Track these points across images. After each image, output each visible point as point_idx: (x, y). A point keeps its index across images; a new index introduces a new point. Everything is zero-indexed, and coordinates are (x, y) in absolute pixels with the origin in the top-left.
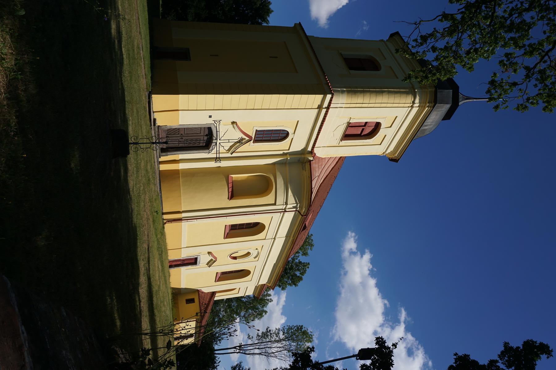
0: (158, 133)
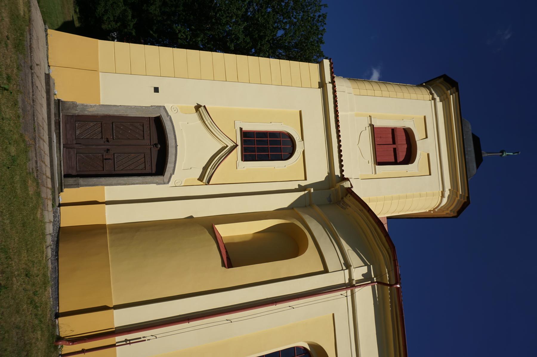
0: (57, 118)
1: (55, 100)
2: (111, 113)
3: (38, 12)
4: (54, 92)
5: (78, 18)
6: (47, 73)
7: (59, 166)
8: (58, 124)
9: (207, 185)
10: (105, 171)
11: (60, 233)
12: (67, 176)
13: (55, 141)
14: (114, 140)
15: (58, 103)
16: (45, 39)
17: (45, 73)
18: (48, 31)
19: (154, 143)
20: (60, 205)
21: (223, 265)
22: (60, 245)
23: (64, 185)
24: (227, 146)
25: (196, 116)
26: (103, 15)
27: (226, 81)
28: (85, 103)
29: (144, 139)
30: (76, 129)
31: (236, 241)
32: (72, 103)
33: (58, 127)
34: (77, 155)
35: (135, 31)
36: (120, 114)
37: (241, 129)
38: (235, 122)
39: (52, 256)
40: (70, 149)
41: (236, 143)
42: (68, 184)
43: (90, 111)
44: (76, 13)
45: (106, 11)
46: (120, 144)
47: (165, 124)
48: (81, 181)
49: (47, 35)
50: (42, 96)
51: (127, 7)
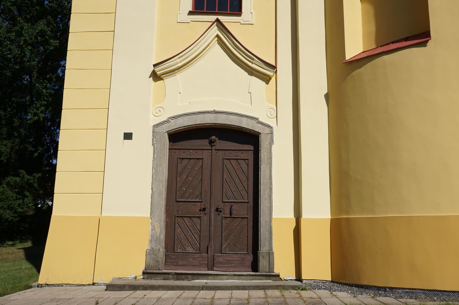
0: (171, 276)
1: (143, 278)
2: (163, 202)
3: (13, 298)
4: (131, 279)
5: (21, 242)
6: (105, 287)
7: (242, 277)
8: (179, 276)
9: (277, 70)
10: (248, 216)
11: (342, 281)
12: (255, 267)
13: (205, 281)
14: (203, 201)
15: (148, 275)
16: (53, 288)
17: (106, 290)
18: (41, 283)
19: (209, 145)
20: (299, 278)
21: (424, 44)
22: (365, 283)
23: (269, 272)
24: (217, 36)
25: (168, 81)
26: (16, 212)
27: (114, 31)
28: (148, 238)
29: (202, 159)
30: (186, 252)
31: (373, 28)
32: (149, 256)
33: (184, 276)
34: (223, 252)
35: (36, 174)
36: (164, 190)
37: (191, 13)
38: (179, 21)
39: (388, 296)
40: (214, 262)
41: (212, 23)
42: (268, 266)
43: (159, 232)
44: (14, 244)
45: (10, 208)
46: (209, 193)
47: (180, 127)
48: (263, 249)
49: (47, 285)
50: (143, 298)
51: (4, 182)
